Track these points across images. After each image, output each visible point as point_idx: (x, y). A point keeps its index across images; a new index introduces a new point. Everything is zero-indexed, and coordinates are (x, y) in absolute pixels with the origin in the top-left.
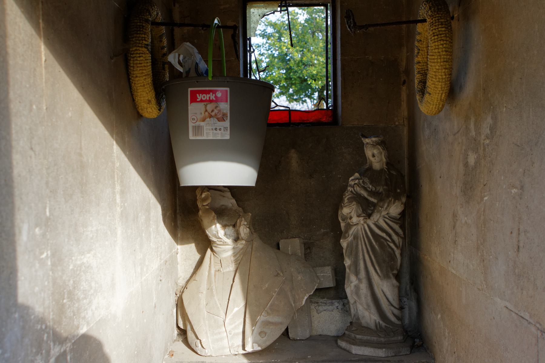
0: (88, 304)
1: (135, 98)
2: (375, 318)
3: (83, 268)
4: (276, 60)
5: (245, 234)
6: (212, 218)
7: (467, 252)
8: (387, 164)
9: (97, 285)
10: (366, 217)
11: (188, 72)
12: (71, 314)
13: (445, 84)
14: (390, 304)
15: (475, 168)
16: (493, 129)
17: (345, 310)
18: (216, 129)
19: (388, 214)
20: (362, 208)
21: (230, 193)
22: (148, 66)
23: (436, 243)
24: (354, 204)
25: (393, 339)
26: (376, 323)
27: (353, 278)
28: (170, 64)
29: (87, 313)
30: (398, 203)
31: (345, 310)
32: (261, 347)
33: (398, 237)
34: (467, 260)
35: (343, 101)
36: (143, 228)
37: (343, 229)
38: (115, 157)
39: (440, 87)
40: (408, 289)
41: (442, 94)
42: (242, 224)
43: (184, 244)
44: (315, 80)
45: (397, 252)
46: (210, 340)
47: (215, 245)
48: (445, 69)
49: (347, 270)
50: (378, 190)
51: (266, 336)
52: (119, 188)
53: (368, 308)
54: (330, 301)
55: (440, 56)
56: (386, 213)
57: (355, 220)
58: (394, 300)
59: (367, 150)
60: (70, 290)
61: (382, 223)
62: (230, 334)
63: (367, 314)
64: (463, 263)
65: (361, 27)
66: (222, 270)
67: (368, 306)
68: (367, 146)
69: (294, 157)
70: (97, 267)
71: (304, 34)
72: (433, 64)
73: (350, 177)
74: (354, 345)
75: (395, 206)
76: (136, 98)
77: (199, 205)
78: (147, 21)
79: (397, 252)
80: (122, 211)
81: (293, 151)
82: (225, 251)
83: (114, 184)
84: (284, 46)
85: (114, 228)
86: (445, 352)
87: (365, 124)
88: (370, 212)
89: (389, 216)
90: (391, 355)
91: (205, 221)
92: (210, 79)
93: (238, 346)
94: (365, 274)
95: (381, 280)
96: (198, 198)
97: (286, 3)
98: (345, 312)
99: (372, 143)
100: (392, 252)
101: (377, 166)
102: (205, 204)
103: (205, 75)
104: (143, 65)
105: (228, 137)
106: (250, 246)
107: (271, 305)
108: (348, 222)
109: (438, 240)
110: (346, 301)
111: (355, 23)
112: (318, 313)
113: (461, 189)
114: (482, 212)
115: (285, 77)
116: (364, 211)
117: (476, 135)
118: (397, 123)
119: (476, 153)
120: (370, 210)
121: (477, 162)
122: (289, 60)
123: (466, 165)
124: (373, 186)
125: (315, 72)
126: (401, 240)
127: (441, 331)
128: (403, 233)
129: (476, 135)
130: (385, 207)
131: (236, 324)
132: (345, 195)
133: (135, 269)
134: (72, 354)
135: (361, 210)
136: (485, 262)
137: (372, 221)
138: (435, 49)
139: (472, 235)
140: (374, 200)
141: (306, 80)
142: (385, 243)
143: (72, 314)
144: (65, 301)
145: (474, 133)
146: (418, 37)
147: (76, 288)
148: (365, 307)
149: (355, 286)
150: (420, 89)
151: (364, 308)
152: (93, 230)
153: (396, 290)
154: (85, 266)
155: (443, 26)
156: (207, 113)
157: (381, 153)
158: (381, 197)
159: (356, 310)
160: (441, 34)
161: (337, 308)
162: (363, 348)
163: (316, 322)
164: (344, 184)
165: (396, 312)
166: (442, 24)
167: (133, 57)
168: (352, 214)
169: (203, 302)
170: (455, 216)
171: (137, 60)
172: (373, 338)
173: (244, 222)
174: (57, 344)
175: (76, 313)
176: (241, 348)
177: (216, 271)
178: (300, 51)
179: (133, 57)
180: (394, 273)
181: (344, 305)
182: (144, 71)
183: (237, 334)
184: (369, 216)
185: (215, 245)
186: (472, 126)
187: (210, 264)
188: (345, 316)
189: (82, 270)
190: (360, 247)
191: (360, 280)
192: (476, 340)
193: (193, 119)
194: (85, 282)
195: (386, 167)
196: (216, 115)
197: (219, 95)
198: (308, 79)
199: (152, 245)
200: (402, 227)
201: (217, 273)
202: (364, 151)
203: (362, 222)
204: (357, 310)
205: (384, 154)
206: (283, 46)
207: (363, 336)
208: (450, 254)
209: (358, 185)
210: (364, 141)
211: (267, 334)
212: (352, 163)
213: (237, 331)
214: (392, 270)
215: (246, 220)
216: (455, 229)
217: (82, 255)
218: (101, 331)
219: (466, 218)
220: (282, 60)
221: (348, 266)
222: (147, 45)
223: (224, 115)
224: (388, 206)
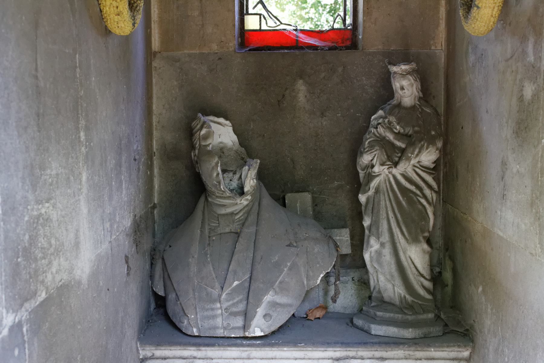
0: (47, 266)
1: (103, 9)
3: (41, 221)
7: (517, 209)
8: (420, 99)
9: (58, 243)
10: (392, 166)
12: (26, 277)
14: (419, 274)
15: (532, 102)
17: (362, 282)
19: (419, 162)
23: (479, 198)
24: (377, 149)
29: (46, 277)
30: (432, 149)
31: (362, 282)
32: (264, 333)
33: (431, 191)
34: (518, 218)
35: (365, 18)
36: (113, 175)
37: (361, 179)
38: (78, 83)
45: (430, 211)
46: (198, 316)
50: (407, 131)
51: (272, 320)
52: (84, 123)
58: (424, 268)
59: (394, 81)
60: (25, 246)
64: (513, 223)
67: (392, 276)
68: (395, 75)
70: (58, 220)
73: (372, 116)
75: (428, 153)
76: (105, 8)
79: (430, 211)
80: (87, 153)
81: (301, 82)
83: (78, 118)
85: (78, 173)
86: (486, 333)
87: (393, 49)
89: (421, 166)
90: (418, 336)
94: (389, 237)
98: (363, 284)
99: (401, 73)
100: (423, 210)
108: (369, 172)
109: (481, 194)
113: (514, 130)
114: (540, 158)
116: (389, 158)
117: (535, 59)
119: (534, 83)
120: (397, 157)
121: (536, 96)
123: (521, 99)
124: (401, 126)
126: (434, 195)
127: (482, 307)
128: (437, 186)
129: (534, 61)
130: (416, 153)
131: (235, 301)
133: (103, 226)
134: (29, 325)
135: (386, 157)
136: (541, 221)
137: (399, 171)
139: (526, 187)
140: (400, 144)
142: (415, 198)
143: (28, 277)
144: (19, 260)
145: (533, 58)
147: (33, 244)
148: (388, 277)
149: (376, 251)
150: (465, 2)
151: (387, 279)
152: (52, 173)
153: (427, 257)
154: (43, 219)
159: (376, 281)
161: (353, 280)
164: (365, 125)
165: (428, 284)
168: (374, 162)
170: (504, 164)
174: (11, 311)
175: (33, 276)
180: (425, 236)
184: (396, 164)
188: (362, 290)
189: (40, 222)
192: (526, 316)
194: (44, 239)
195: (418, 103)
199: (124, 197)
204: (378, 281)
205: (416, 86)
207: (385, 313)
208: (496, 212)
210: (391, 70)
211: (273, 318)
212: (374, 98)
214: (423, 231)
216: (503, 180)
217: (40, 204)
218: (63, 300)
219: (518, 166)
221: (368, 227)
224: (419, 152)
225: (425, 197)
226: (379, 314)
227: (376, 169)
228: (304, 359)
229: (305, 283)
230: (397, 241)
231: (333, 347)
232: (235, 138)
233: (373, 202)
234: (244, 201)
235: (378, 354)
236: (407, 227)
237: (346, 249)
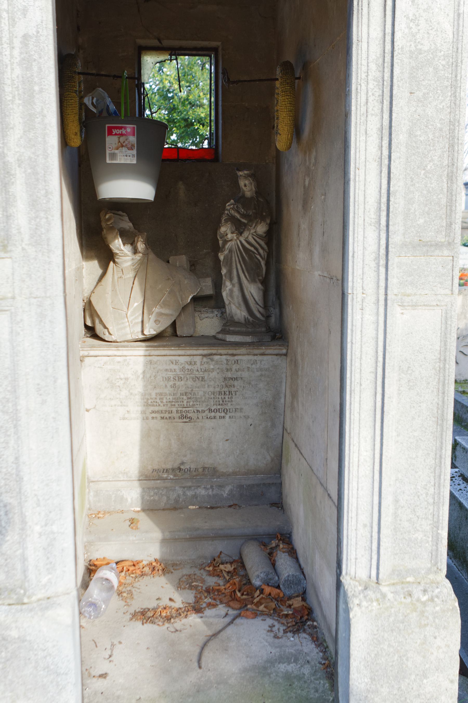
2: (245, 314)
4: (157, 97)
5: (142, 249)
6: (115, 234)
8: (256, 192)
11: (101, 112)
13: (290, 128)
16: (316, 159)
18: (126, 156)
19: (255, 232)
20: (235, 226)
21: (127, 218)
22: (76, 107)
25: (258, 330)
26: (245, 318)
27: (228, 284)
28: (86, 105)
39: (286, 129)
40: (274, 300)
41: (288, 135)
42: (139, 240)
43: (88, 261)
44: (203, 126)
47: (118, 257)
48: (290, 116)
49: (224, 278)
53: (239, 307)
54: (211, 310)
55: (286, 107)
56: (254, 231)
57: (230, 236)
58: (259, 300)
61: (251, 239)
62: (131, 323)
63: (238, 312)
65: (234, 82)
66: (123, 276)
67: (239, 304)
69: (181, 187)
71: (192, 66)
72: (281, 113)
74: (228, 334)
77: (103, 225)
78: (75, 72)
81: (181, 183)
82: (126, 261)
84: (166, 79)
88: (242, 230)
91: (109, 237)
92: (123, 118)
93: (138, 332)
95: (249, 283)
96: (102, 219)
97: (175, 52)
101: (248, 194)
102: (109, 223)
103: (114, 115)
104: (73, 106)
105: (135, 162)
106: (146, 258)
107: (164, 301)
110: (224, 310)
111: (229, 79)
112: (201, 320)
115: (167, 118)
116: (237, 229)
118: (267, 161)
122: (172, 98)
125: (203, 115)
130: (253, 226)
131: (136, 315)
132: (222, 217)
138: (283, 102)
140: (245, 221)
141: (192, 124)
146: (277, 91)
148: (237, 305)
149: (230, 290)
153: (261, 293)
155: (289, 85)
156: (120, 144)
157: (251, 184)
158: (251, 219)
160: (287, 91)
162: (235, 336)
163: (199, 328)
165: (261, 310)
166: (288, 84)
167: (66, 100)
169: (109, 301)
171: (69, 102)
172: (242, 329)
173: (140, 239)
176: (140, 333)
177: (118, 278)
178: (187, 87)
179: (66, 100)
181: (222, 313)
182: (74, 111)
183: (138, 323)
184: (241, 234)
185: (118, 257)
186: (307, 159)
187: (113, 271)
190: (234, 258)
191: (233, 285)
193: (110, 148)
196: (126, 145)
197: (129, 130)
198: (195, 123)
200: (267, 244)
201: (119, 279)
202: (238, 181)
203: (235, 238)
206: (164, 80)
209: (233, 209)
210: (238, 174)
213: (137, 321)
215: (142, 238)
220: (164, 97)
222: (76, 91)
223: (133, 145)
224: (256, 225)
226: (231, 329)
228: (184, 355)
229: (181, 303)
230: (242, 283)
231: (202, 347)
233: (228, 260)
235: (230, 352)
236: (248, 273)
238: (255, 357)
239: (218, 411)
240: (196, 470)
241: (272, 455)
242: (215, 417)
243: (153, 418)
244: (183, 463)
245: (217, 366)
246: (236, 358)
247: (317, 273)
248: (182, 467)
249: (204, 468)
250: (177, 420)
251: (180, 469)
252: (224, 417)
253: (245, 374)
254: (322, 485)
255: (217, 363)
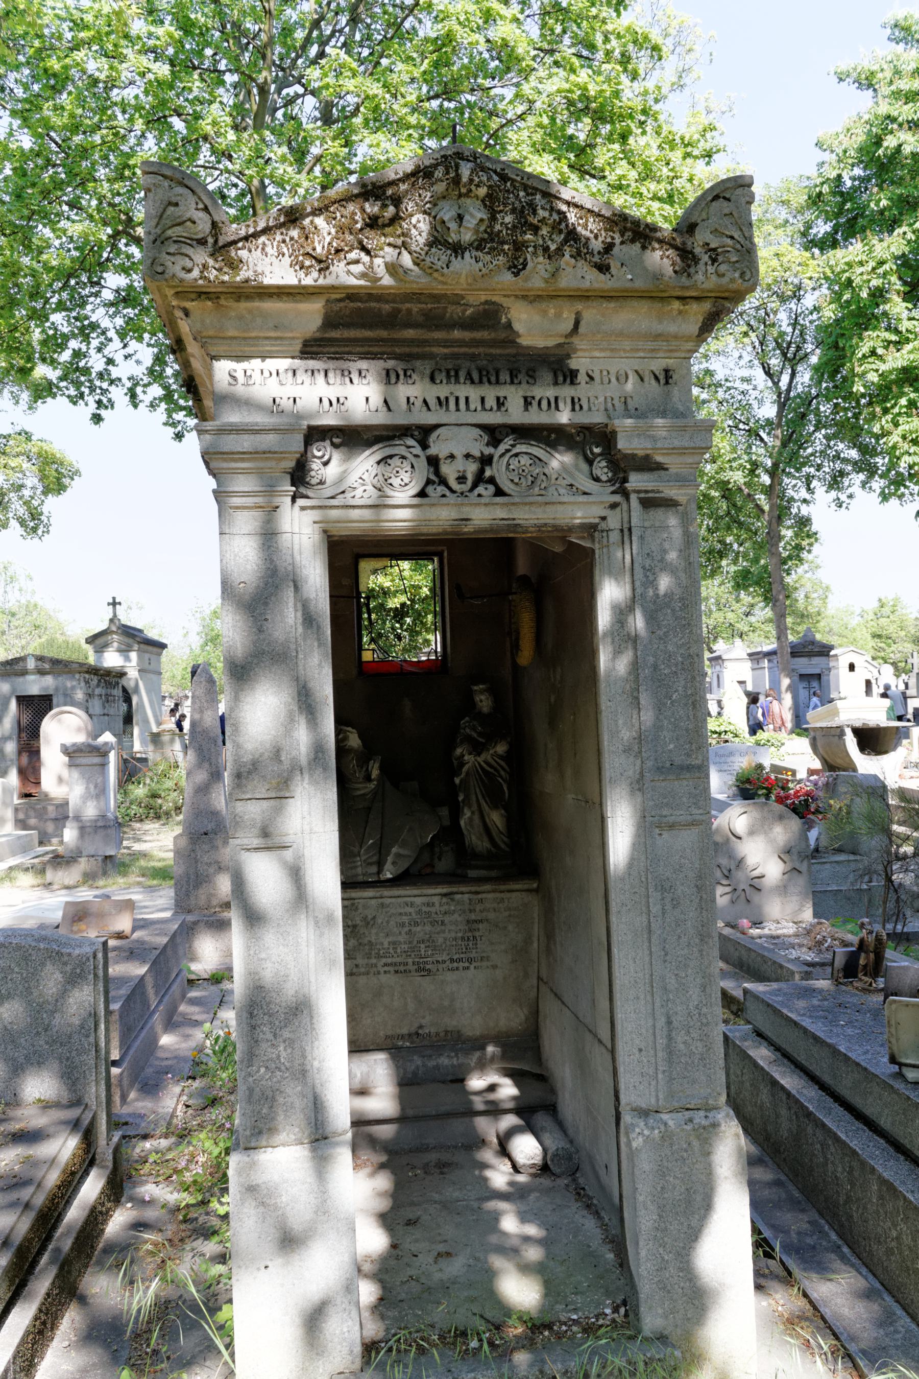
61: (490, 760)
101: (485, 710)
165: (505, 839)
184: (479, 754)
225: (501, 777)
227: (466, 758)
232: (359, 742)
234: (372, 786)
235: (473, 889)
237: (447, 822)
238: (502, 895)
239: (461, 960)
240: (437, 1034)
241: (526, 1011)
242: (457, 969)
243: (385, 972)
244: (421, 1027)
245: (459, 907)
246: (480, 896)
247: (570, 796)
248: (420, 1032)
249: (446, 1032)
250: (414, 973)
251: (417, 1034)
252: (468, 968)
253: (491, 916)
254: (590, 1031)
255: (458, 902)
